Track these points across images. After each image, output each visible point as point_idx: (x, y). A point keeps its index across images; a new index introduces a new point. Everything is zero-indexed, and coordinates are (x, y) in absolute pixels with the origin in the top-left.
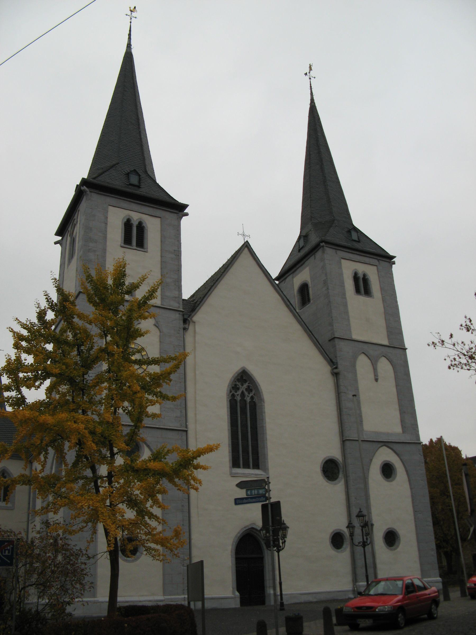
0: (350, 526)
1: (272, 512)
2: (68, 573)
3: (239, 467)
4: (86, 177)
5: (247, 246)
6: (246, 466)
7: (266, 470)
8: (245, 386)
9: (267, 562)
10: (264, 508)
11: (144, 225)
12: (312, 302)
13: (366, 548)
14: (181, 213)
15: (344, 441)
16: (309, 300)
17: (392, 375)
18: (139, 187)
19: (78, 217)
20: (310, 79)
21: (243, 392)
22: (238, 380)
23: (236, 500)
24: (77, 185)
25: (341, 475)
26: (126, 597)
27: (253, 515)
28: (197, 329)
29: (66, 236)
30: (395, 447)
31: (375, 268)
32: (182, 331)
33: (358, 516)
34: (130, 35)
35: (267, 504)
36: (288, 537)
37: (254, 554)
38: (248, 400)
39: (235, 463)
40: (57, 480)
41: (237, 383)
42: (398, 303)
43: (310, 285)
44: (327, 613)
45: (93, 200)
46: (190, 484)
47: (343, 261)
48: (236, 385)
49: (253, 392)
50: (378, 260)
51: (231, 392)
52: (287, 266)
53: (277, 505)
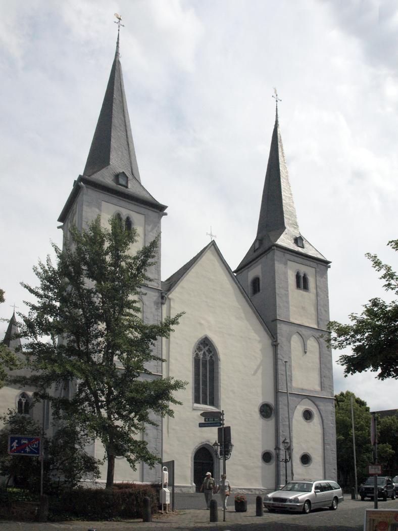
0: (277, 448)
1: (225, 435)
3: (199, 403)
4: (82, 174)
5: (213, 244)
6: (205, 403)
7: (217, 406)
9: (216, 466)
10: (220, 430)
11: (131, 220)
12: (261, 291)
13: (287, 463)
14: (161, 213)
15: (277, 392)
16: (259, 291)
17: (318, 350)
18: (127, 187)
19: (76, 208)
20: (277, 101)
22: (201, 344)
23: (200, 424)
24: (75, 181)
25: (273, 415)
26: (117, 480)
27: (211, 435)
28: (172, 305)
29: (67, 222)
30: (312, 398)
31: (314, 269)
32: (160, 305)
33: (284, 442)
34: (118, 43)
35: (221, 428)
36: (233, 451)
37: (206, 461)
39: (197, 400)
40: (8, 362)
41: (201, 346)
42: (329, 298)
44: (259, 500)
45: (88, 194)
46: (163, 410)
48: (199, 347)
49: (212, 353)
50: (317, 264)
51: (196, 351)
52: (244, 263)
53: (228, 429)
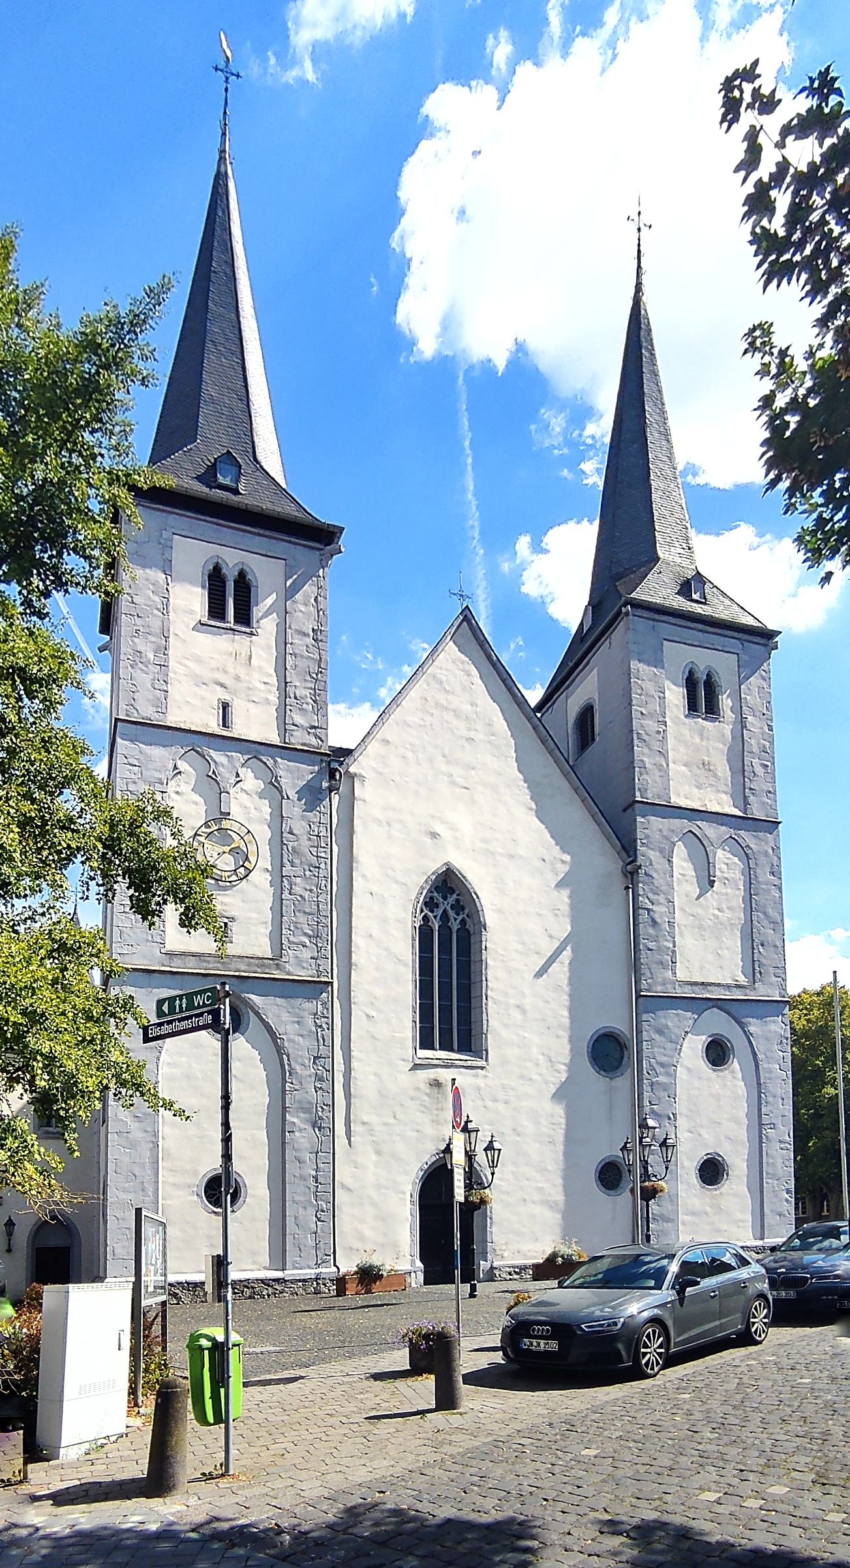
2: (20, 316)
8: (452, 899)
21: (445, 911)
30: (728, 1006)
38: (455, 926)
41: (435, 894)
43: (596, 707)
47: (665, 643)
48: (431, 898)
